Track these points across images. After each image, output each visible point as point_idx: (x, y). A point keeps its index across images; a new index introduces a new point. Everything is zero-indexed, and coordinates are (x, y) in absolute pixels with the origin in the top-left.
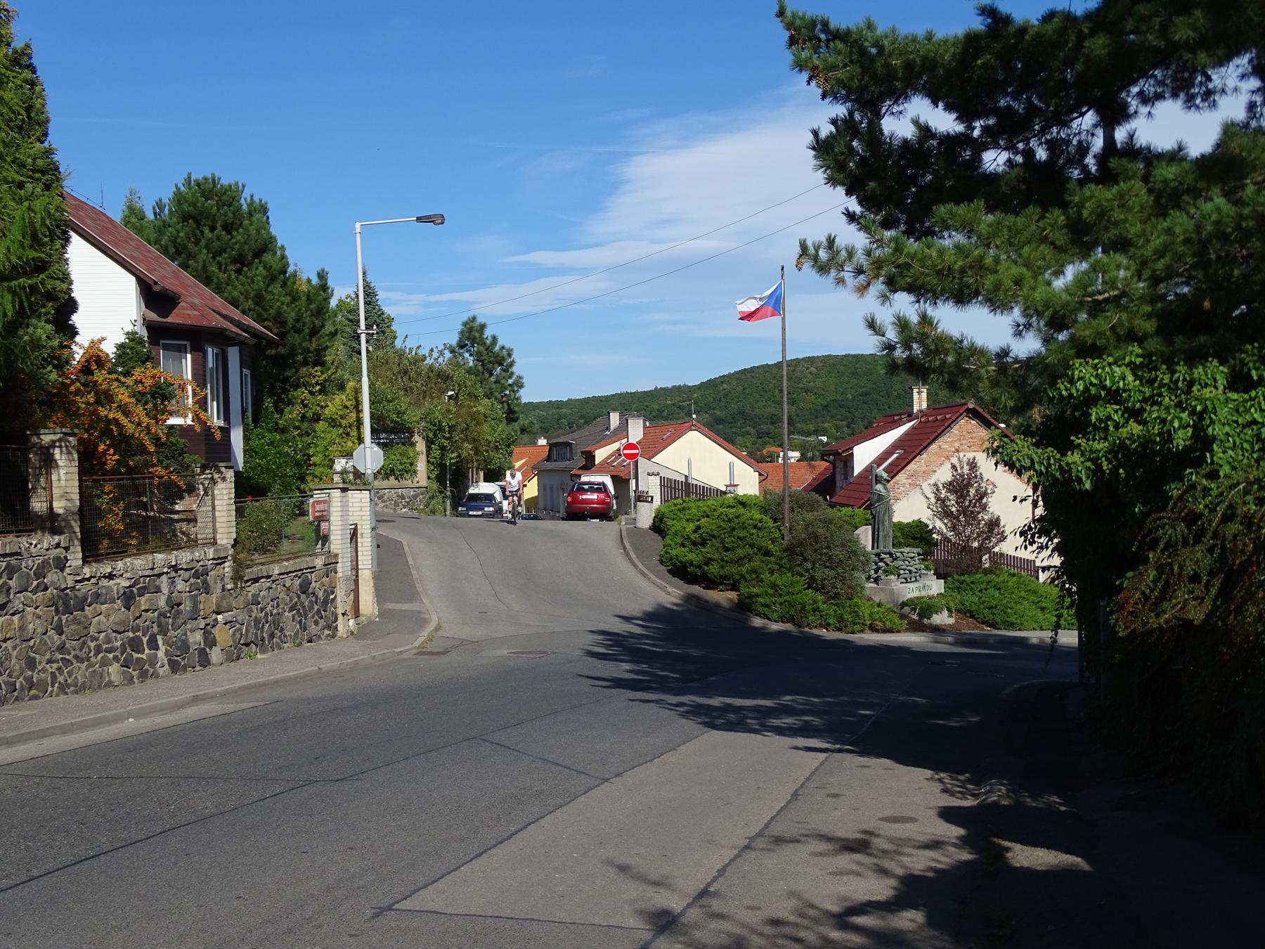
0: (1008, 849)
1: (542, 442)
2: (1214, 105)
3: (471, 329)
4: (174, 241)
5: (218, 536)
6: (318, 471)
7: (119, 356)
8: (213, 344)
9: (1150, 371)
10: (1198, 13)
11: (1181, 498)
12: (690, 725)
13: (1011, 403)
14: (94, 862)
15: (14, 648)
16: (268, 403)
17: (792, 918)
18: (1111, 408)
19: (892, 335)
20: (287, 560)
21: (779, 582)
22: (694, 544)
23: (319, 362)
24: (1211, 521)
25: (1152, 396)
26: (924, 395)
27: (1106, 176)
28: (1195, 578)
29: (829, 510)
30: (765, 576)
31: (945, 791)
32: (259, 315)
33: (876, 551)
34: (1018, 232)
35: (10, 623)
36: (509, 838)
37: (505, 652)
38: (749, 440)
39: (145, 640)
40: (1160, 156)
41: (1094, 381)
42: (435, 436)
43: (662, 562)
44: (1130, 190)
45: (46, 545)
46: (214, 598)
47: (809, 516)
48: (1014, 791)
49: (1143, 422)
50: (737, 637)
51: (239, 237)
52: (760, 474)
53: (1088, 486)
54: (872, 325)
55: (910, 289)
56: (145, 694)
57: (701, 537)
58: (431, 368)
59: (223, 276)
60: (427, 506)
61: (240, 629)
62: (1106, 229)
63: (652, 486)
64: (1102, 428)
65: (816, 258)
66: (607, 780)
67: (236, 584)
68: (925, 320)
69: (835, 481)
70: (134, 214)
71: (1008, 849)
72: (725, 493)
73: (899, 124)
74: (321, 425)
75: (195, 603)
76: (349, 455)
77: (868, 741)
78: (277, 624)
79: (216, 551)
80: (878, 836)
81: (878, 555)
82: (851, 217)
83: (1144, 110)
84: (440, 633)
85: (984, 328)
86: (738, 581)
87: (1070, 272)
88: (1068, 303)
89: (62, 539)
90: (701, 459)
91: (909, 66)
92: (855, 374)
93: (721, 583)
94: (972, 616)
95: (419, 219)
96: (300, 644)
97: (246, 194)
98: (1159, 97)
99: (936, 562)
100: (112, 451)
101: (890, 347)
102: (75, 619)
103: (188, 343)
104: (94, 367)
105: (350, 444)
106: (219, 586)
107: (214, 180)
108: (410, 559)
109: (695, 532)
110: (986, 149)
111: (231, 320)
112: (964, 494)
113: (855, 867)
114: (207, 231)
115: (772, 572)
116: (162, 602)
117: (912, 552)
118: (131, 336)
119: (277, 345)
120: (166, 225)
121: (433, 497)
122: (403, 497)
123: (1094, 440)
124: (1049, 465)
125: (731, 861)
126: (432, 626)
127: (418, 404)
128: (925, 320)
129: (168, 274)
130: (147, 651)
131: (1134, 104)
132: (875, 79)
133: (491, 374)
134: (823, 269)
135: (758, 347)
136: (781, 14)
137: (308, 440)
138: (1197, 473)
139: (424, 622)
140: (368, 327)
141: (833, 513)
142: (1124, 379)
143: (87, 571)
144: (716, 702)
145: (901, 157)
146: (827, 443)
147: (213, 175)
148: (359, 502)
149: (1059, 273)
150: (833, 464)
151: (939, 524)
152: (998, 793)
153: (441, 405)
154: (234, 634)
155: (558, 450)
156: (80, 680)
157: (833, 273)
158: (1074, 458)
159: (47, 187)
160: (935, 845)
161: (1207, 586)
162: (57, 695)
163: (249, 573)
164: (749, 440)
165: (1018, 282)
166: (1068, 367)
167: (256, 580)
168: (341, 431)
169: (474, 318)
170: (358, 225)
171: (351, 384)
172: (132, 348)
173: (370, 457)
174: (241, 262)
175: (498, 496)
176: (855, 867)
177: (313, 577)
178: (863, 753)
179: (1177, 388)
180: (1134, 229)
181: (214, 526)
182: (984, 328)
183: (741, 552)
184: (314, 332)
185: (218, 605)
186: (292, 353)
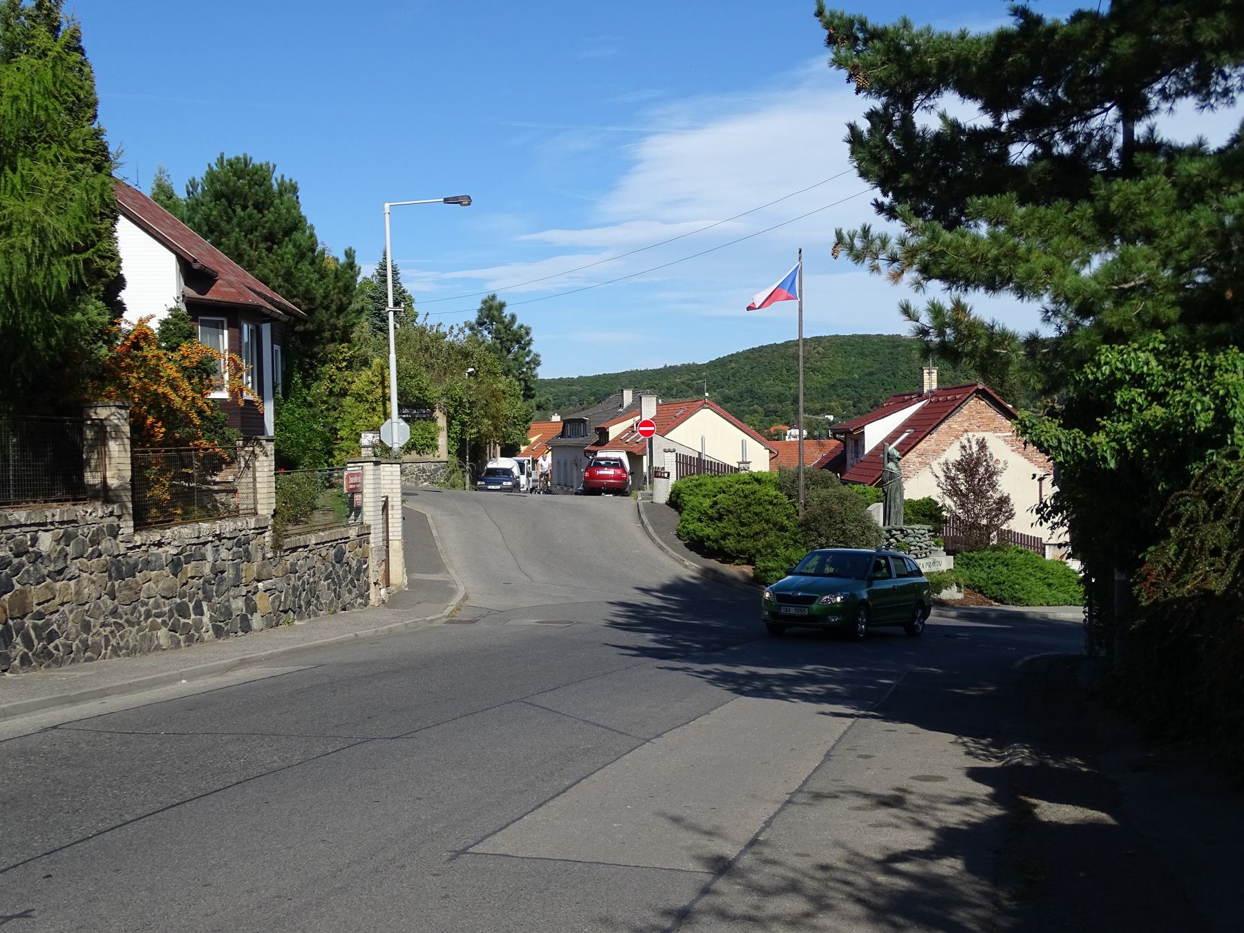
0: (1035, 806)
1: (556, 418)
2: (1232, 102)
3: (490, 308)
4: (207, 219)
5: (259, 507)
6: (345, 444)
7: (162, 332)
8: (248, 321)
9: (1172, 357)
10: (1221, 16)
11: (1202, 477)
12: (719, 692)
13: (1039, 386)
14: (182, 808)
15: (71, 612)
16: (297, 378)
17: (840, 865)
18: (1135, 392)
19: (926, 320)
20: (323, 530)
21: (794, 557)
22: (711, 519)
23: (346, 338)
24: (1231, 499)
25: (1175, 381)
26: (934, 376)
27: (1129, 169)
28: (1216, 552)
29: (842, 487)
30: (781, 551)
31: (969, 753)
32: (288, 292)
33: (887, 527)
34: (1048, 223)
35: (67, 588)
36: (564, 791)
37: (533, 621)
38: (757, 418)
39: (191, 605)
40: (1180, 151)
41: (1119, 365)
42: (456, 411)
43: (679, 536)
44: (1156, 184)
45: (100, 513)
46: (255, 567)
47: (824, 493)
48: (1036, 754)
49: (1166, 405)
50: (789, 603)
51: (270, 215)
52: (771, 452)
53: (1112, 465)
54: (906, 310)
55: (943, 277)
56: (193, 657)
57: (718, 512)
58: (451, 346)
59: (254, 254)
60: (447, 480)
61: (279, 597)
62: (1132, 221)
63: (668, 463)
64: (1126, 410)
65: (851, 247)
66: (648, 741)
67: (275, 552)
68: (959, 307)
69: (845, 458)
70: (164, 193)
71: (1035, 806)
72: (737, 470)
73: (927, 120)
74: (348, 400)
75: (238, 571)
76: (376, 429)
77: (893, 707)
78: (313, 592)
79: (257, 520)
80: (911, 793)
81: (889, 531)
82: (880, 207)
83: (1165, 106)
84: (467, 603)
85: (1017, 315)
86: (754, 556)
87: (1097, 262)
88: (1096, 292)
89: (116, 508)
90: (713, 436)
91: (943, 64)
92: (862, 355)
93: (737, 557)
94: (981, 592)
95: (446, 201)
96: (335, 612)
97: (277, 175)
98: (1179, 94)
99: (945, 538)
100: (160, 424)
101: (923, 332)
102: (127, 585)
103: (225, 320)
104: (143, 344)
105: (376, 419)
106: (260, 555)
107: (245, 160)
108: (434, 532)
109: (712, 507)
110: (1013, 142)
111: (265, 297)
112: (974, 473)
113: (893, 821)
114: (239, 210)
115: (787, 547)
116: (207, 569)
117: (923, 528)
118: (174, 312)
119: (306, 322)
120: (198, 204)
121: (453, 472)
122: (424, 471)
123: (1119, 421)
124: (1075, 445)
125: (776, 814)
126: (460, 595)
127: (439, 380)
128: (959, 307)
129: (205, 253)
130: (193, 616)
131: (1154, 100)
132: (910, 76)
133: (509, 352)
134: (858, 257)
135: (778, 327)
136: (820, 13)
137: (334, 414)
138: (1218, 454)
139: (452, 592)
140: (396, 304)
141: (845, 490)
142: (1147, 363)
143: (138, 539)
144: (741, 670)
145: (933, 150)
146: (834, 422)
147: (245, 155)
148: (390, 475)
149: (1086, 261)
150: (844, 442)
151: (949, 502)
152: (1022, 755)
153: (461, 383)
154: (273, 602)
155: (572, 426)
156: (131, 644)
157: (868, 261)
158: (1100, 438)
159: (98, 168)
160: (966, 801)
161: (1228, 559)
162: (110, 658)
163: (288, 543)
164: (757, 418)
165: (1049, 271)
166: (1095, 352)
167: (294, 550)
168: (367, 406)
169: (494, 297)
170: (387, 205)
171: (377, 360)
172: (175, 324)
173: (397, 432)
174: (271, 239)
175: (516, 471)
176: (893, 821)
177: (347, 547)
178: (888, 718)
179: (1199, 373)
180: (1159, 221)
181: (255, 497)
182: (1017, 315)
183: (756, 528)
184: (342, 309)
185: (259, 573)
186: (320, 330)
